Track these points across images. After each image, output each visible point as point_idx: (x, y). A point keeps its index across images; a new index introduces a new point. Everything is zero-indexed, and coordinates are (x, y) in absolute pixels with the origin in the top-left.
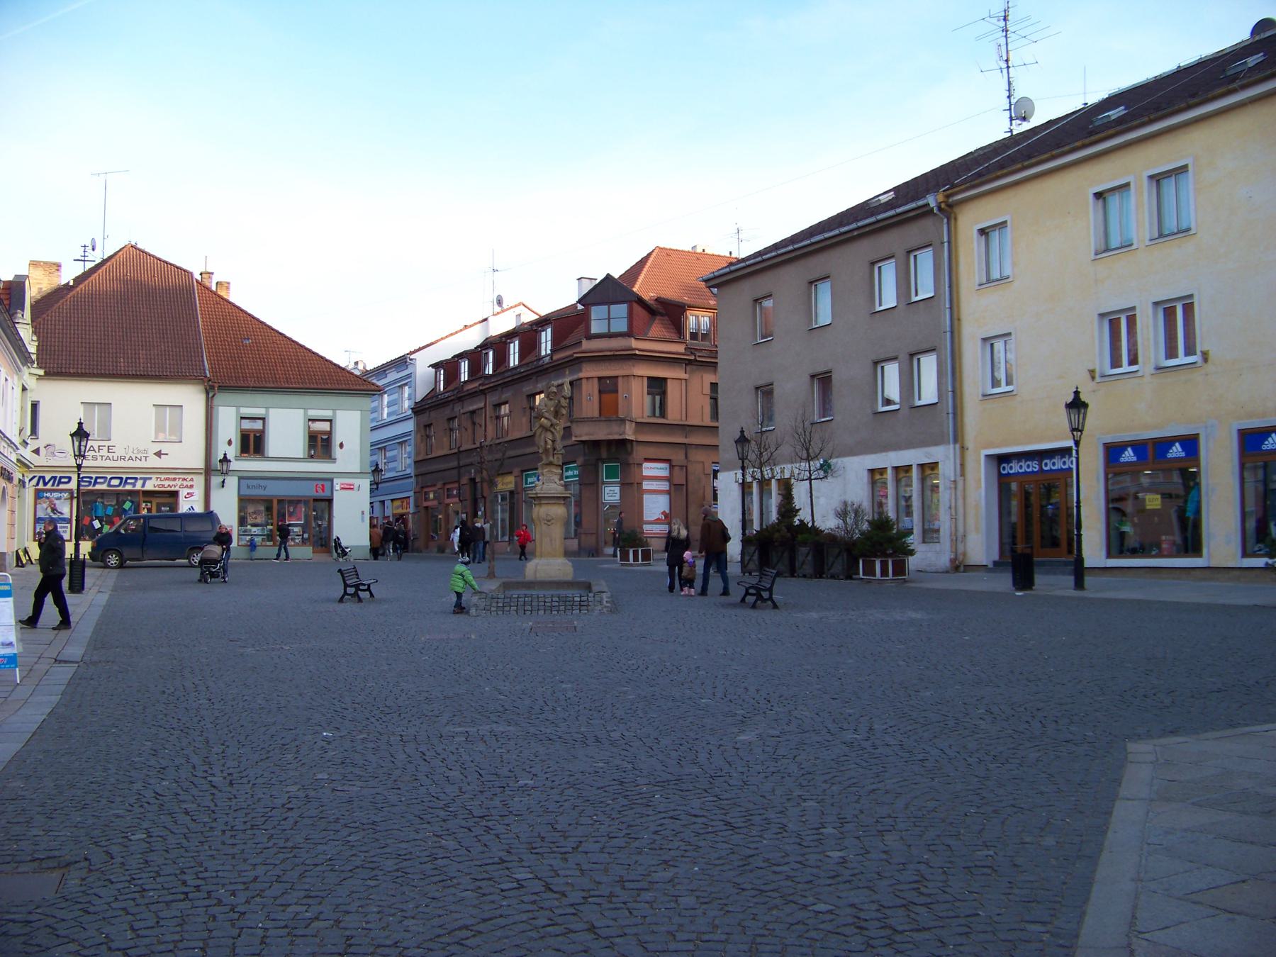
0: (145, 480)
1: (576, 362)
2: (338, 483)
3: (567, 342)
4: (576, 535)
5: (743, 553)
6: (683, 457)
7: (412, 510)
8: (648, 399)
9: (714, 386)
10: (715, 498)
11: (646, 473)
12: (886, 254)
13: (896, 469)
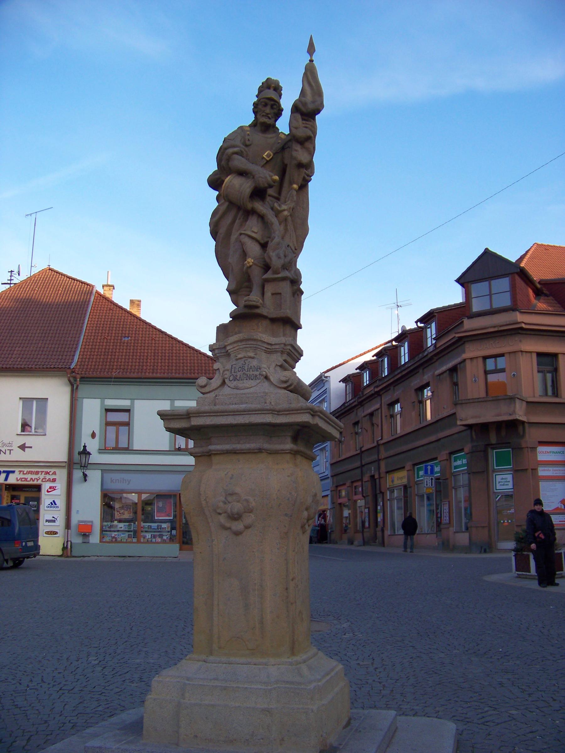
0: (8, 473)
1: (460, 342)
4: (467, 529)
8: (538, 377)
11: (540, 457)
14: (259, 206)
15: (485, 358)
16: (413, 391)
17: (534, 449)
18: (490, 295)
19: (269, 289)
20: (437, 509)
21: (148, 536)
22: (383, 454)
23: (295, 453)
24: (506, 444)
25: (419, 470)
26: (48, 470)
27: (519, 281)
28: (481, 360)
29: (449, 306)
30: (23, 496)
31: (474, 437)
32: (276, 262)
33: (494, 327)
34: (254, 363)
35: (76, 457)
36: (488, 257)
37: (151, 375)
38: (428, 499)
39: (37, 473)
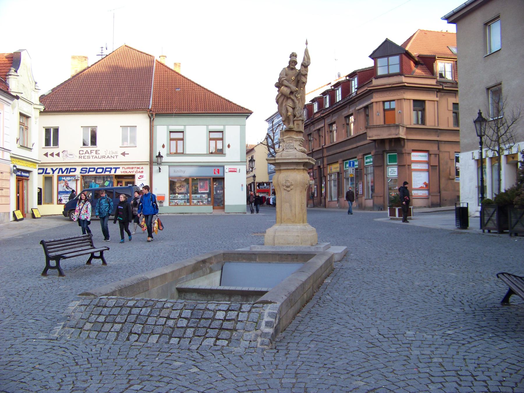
0: (116, 169)
1: (370, 93)
2: (227, 168)
4: (372, 197)
5: (482, 213)
6: (437, 149)
8: (414, 113)
9: (456, 105)
10: (458, 173)
11: (413, 159)
14: (292, 97)
15: (384, 102)
16: (343, 118)
17: (409, 154)
18: (388, 65)
19: (296, 123)
20: (356, 186)
21: (195, 201)
22: (326, 154)
23: (303, 169)
24: (395, 151)
25: (346, 163)
26: (139, 166)
27: (405, 58)
28: (381, 103)
29: (365, 68)
30: (124, 181)
31: (377, 146)
32: (298, 115)
33: (390, 84)
34: (292, 144)
35: (155, 159)
36: (387, 42)
37: (195, 112)
38: (351, 180)
39: (132, 168)
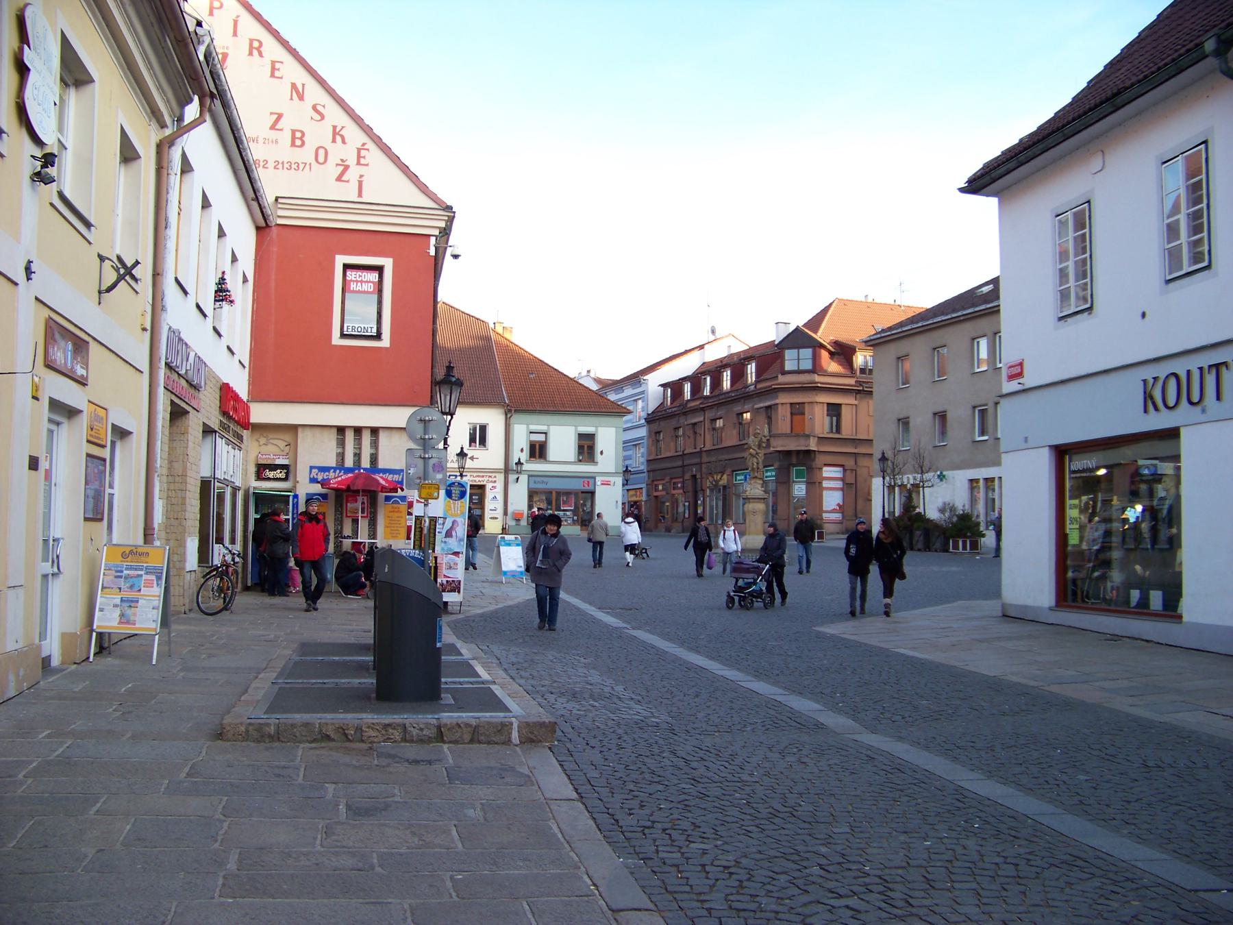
2: (599, 480)
3: (765, 376)
7: (644, 498)
8: (827, 419)
11: (825, 475)
12: (981, 333)
13: (986, 479)
22: (705, 459)
